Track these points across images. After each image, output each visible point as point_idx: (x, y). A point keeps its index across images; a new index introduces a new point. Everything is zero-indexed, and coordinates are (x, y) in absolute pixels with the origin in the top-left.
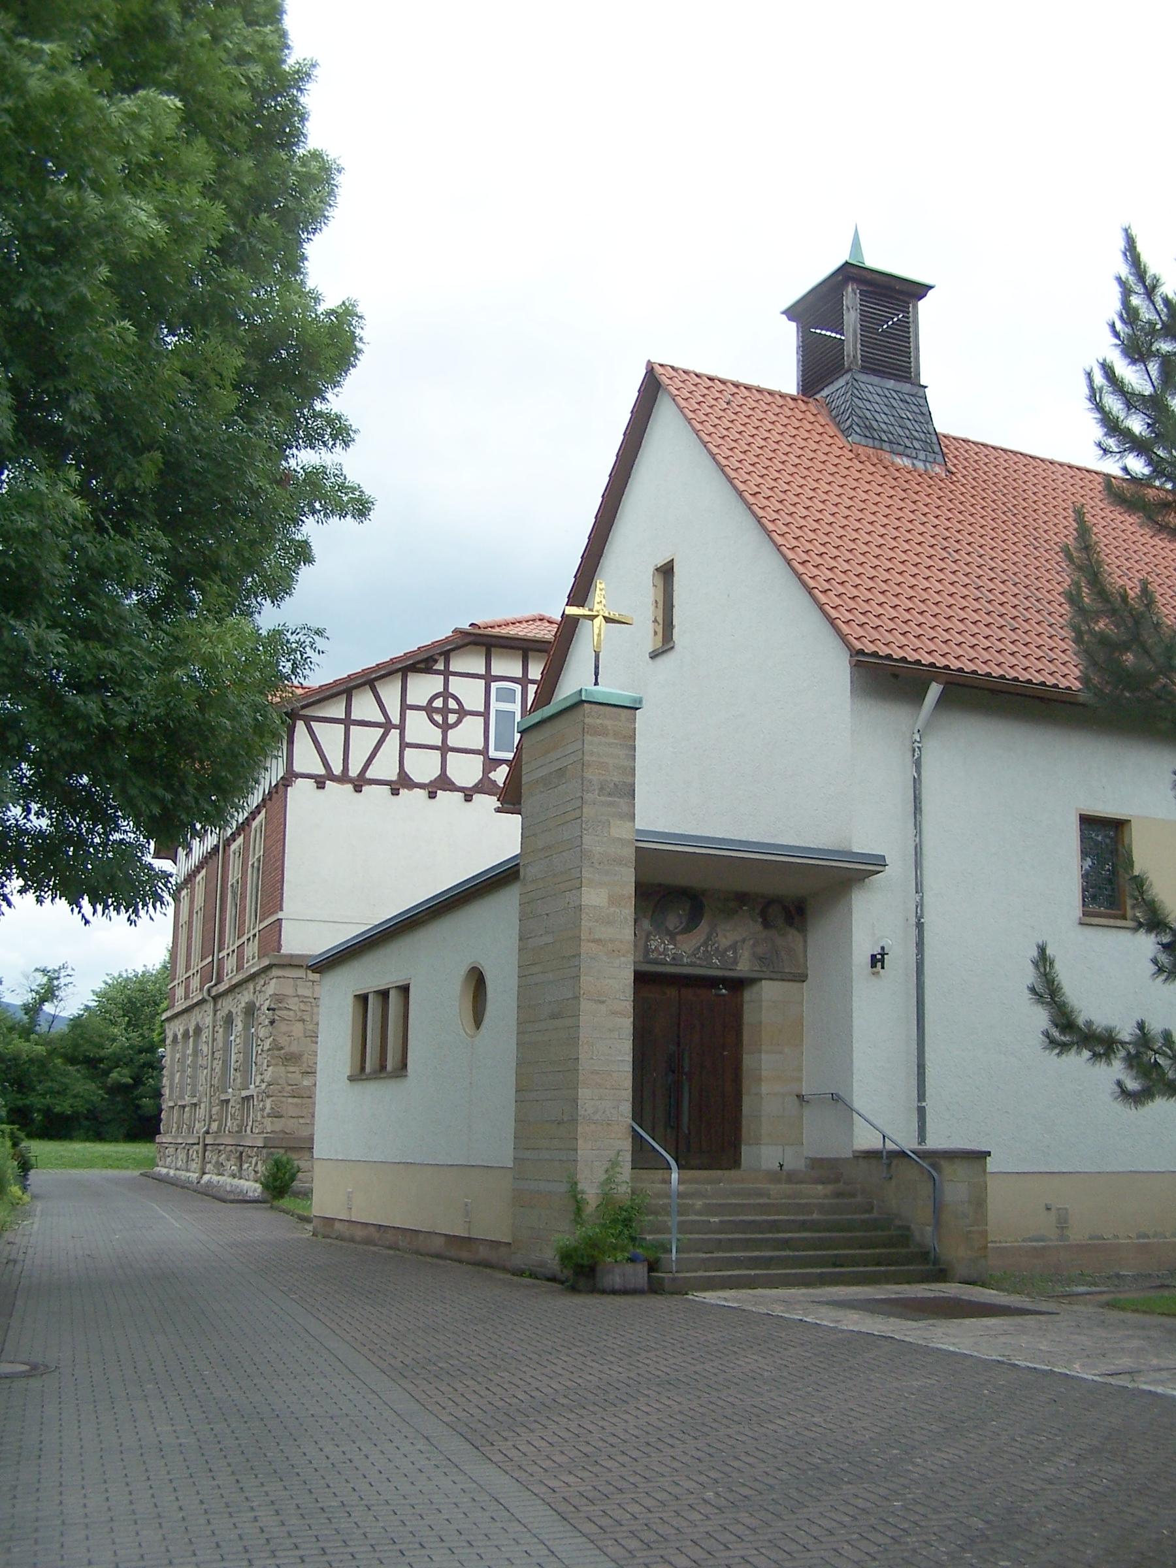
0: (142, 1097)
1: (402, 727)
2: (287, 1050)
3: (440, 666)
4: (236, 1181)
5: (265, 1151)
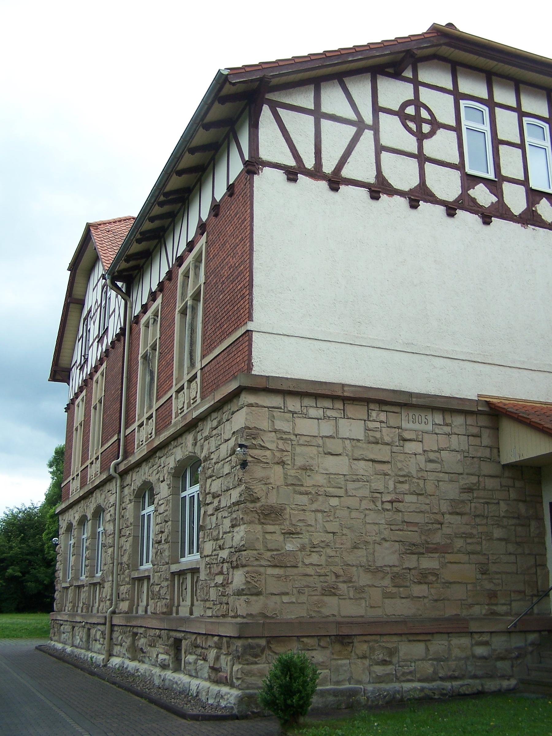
0: (29, 581)
1: (375, 128)
3: (408, 74)
4: (169, 674)
5: (239, 643)
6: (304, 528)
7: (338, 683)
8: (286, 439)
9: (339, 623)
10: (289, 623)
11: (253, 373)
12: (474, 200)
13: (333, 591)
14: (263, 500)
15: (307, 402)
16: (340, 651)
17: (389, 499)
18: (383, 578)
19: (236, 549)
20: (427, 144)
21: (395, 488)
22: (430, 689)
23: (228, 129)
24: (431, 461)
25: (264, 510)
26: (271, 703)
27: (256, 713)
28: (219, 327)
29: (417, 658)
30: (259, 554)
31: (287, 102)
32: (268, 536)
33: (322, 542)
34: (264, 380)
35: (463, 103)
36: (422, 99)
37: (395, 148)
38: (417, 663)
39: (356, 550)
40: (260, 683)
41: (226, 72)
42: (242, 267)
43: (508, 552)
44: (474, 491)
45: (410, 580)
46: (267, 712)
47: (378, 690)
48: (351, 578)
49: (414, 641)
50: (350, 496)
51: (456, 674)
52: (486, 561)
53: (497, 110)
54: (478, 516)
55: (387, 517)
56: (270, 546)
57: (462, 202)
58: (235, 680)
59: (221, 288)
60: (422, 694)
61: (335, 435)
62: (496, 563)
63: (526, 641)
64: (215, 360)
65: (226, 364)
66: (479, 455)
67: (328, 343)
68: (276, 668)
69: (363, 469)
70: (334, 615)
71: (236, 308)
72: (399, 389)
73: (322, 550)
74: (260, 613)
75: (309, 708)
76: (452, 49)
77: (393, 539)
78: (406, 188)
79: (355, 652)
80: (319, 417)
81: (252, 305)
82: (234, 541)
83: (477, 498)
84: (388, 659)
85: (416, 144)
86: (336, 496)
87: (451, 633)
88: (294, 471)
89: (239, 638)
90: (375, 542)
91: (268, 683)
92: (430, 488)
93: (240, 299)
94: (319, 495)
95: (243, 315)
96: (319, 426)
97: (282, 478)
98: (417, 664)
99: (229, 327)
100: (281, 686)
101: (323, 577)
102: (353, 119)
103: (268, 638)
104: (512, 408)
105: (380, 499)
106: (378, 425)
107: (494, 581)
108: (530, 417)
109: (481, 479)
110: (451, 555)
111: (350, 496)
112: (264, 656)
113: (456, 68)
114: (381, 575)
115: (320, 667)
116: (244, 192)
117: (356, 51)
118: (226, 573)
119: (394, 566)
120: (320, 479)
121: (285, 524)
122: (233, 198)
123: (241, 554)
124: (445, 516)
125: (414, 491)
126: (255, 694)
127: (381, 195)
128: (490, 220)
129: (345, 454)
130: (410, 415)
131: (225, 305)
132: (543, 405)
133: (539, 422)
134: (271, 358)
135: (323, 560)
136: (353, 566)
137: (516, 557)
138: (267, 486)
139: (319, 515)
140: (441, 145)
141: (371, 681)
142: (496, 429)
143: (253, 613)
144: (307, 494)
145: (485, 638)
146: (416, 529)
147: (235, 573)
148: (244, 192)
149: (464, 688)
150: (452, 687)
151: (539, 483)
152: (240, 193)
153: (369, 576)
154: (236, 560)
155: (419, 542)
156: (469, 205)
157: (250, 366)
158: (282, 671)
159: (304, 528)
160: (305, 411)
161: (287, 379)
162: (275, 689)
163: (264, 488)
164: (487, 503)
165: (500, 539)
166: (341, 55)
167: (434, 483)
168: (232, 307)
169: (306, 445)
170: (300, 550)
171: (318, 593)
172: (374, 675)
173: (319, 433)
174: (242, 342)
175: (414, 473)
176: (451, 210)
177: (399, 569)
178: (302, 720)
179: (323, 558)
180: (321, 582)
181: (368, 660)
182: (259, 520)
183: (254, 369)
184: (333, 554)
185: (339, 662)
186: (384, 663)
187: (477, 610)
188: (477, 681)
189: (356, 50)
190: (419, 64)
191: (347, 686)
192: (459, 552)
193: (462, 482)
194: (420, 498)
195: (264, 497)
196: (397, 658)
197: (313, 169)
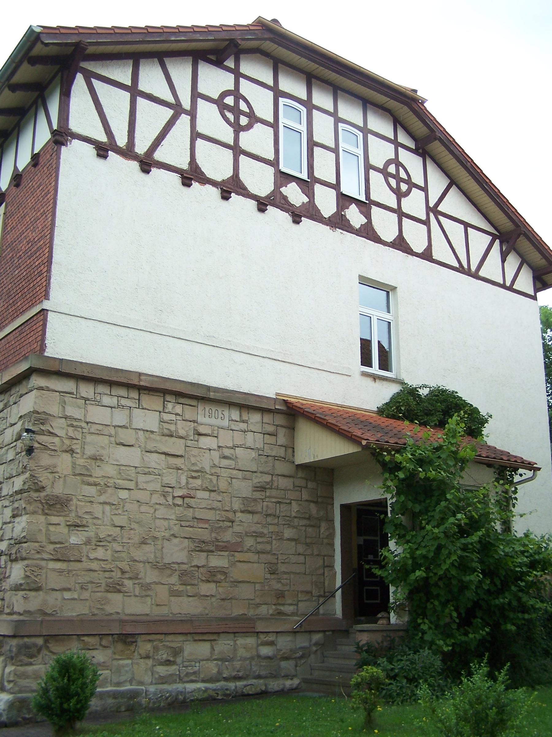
1: (193, 114)
2: (48, 491)
5: (14, 642)
6: (90, 521)
7: (118, 684)
8: (76, 427)
9: (122, 622)
10: (69, 621)
11: (46, 354)
12: (285, 198)
13: (118, 587)
14: (48, 491)
15: (101, 389)
16: (122, 651)
17: (181, 494)
18: (170, 575)
19: (16, 541)
20: (243, 135)
21: (187, 483)
22: (214, 690)
23: (36, 94)
24: (225, 457)
25: (48, 500)
26: (45, 708)
27: (28, 719)
28: (12, 305)
29: (201, 658)
30: (41, 546)
31: (103, 74)
32: (52, 528)
33: (109, 536)
34: (57, 362)
35: (282, 101)
36: (242, 91)
37: (212, 136)
38: (201, 663)
39: (144, 546)
40: (34, 685)
41: (38, 30)
42: (42, 242)
43: (297, 553)
44: (267, 490)
45: (199, 578)
46: (40, 718)
47: (160, 692)
48: (138, 574)
49: (200, 640)
50: (140, 489)
51: (241, 674)
52: (276, 561)
53: (315, 112)
54: (270, 515)
55: (177, 512)
56: (53, 539)
57: (274, 199)
58: (6, 684)
59: (17, 264)
60: (206, 695)
61: (128, 425)
62: (286, 563)
63: (311, 641)
64: (6, 339)
65: (17, 344)
66: (274, 454)
67: (128, 330)
68: (53, 669)
69: (156, 462)
70: (118, 613)
71: (32, 285)
72: (197, 382)
73: (108, 544)
74: (39, 610)
75: (87, 712)
76: (276, 46)
77: (183, 535)
78: (219, 178)
79: (138, 652)
80: (113, 406)
81: (49, 283)
82: (14, 533)
83: (270, 497)
84: (172, 659)
85: (232, 135)
86: (126, 489)
87: (238, 633)
88: (83, 460)
89: (14, 636)
90: (164, 538)
91: (43, 685)
92: (223, 485)
93: (37, 276)
94: (109, 487)
95: (39, 292)
96: (112, 416)
97: (70, 467)
98: (201, 664)
99: (23, 305)
100: (57, 689)
101: (108, 573)
102: (171, 101)
103: (46, 637)
104: (309, 408)
105: (171, 494)
106: (173, 417)
107: (282, 581)
108: (327, 418)
109: (274, 478)
110: (241, 554)
111: (140, 489)
112: (40, 657)
113: (278, 65)
114: (168, 572)
115: (99, 668)
116: (50, 163)
117: (180, 32)
118: (3, 566)
119: (183, 563)
120: (110, 470)
121: (70, 515)
122: (37, 169)
123: (22, 547)
124: (236, 514)
125: (207, 487)
126: (28, 698)
127: (193, 182)
128: (299, 220)
129: (137, 446)
130: (207, 409)
131: (20, 282)
132: (340, 408)
133: (336, 424)
134: (64, 342)
135: (108, 555)
136: (141, 562)
137: (305, 558)
138: (54, 474)
139: (107, 508)
140: (257, 139)
141: (154, 682)
142: (292, 429)
143: (32, 609)
144: (95, 485)
145: (271, 638)
146: (206, 526)
147: (13, 566)
148: (50, 163)
149: (248, 688)
150: (236, 687)
151: (331, 485)
152: (45, 164)
153: (156, 572)
154: (16, 553)
155: (209, 539)
156: (280, 202)
157: (43, 347)
158: (60, 672)
159: (90, 521)
160: (98, 398)
161: (81, 363)
162: (51, 692)
163: (50, 476)
164: (279, 503)
165: (289, 540)
166: (164, 33)
167: (227, 480)
168: (28, 283)
169: (97, 434)
170: (85, 544)
171: (103, 590)
172: (157, 676)
173: (112, 423)
174: (36, 321)
175: (208, 469)
176: (262, 205)
177: (187, 566)
178: (78, 725)
179: (109, 552)
180: (106, 578)
181: (151, 660)
182: (43, 510)
183: (47, 350)
184: (119, 548)
185: (121, 662)
186: (168, 663)
187: (264, 610)
188: (261, 681)
189: (179, 30)
190: (242, 56)
191: (128, 687)
192: (249, 550)
193: (256, 481)
194: (213, 494)
195: (49, 487)
196: (181, 658)
197: (125, 148)
